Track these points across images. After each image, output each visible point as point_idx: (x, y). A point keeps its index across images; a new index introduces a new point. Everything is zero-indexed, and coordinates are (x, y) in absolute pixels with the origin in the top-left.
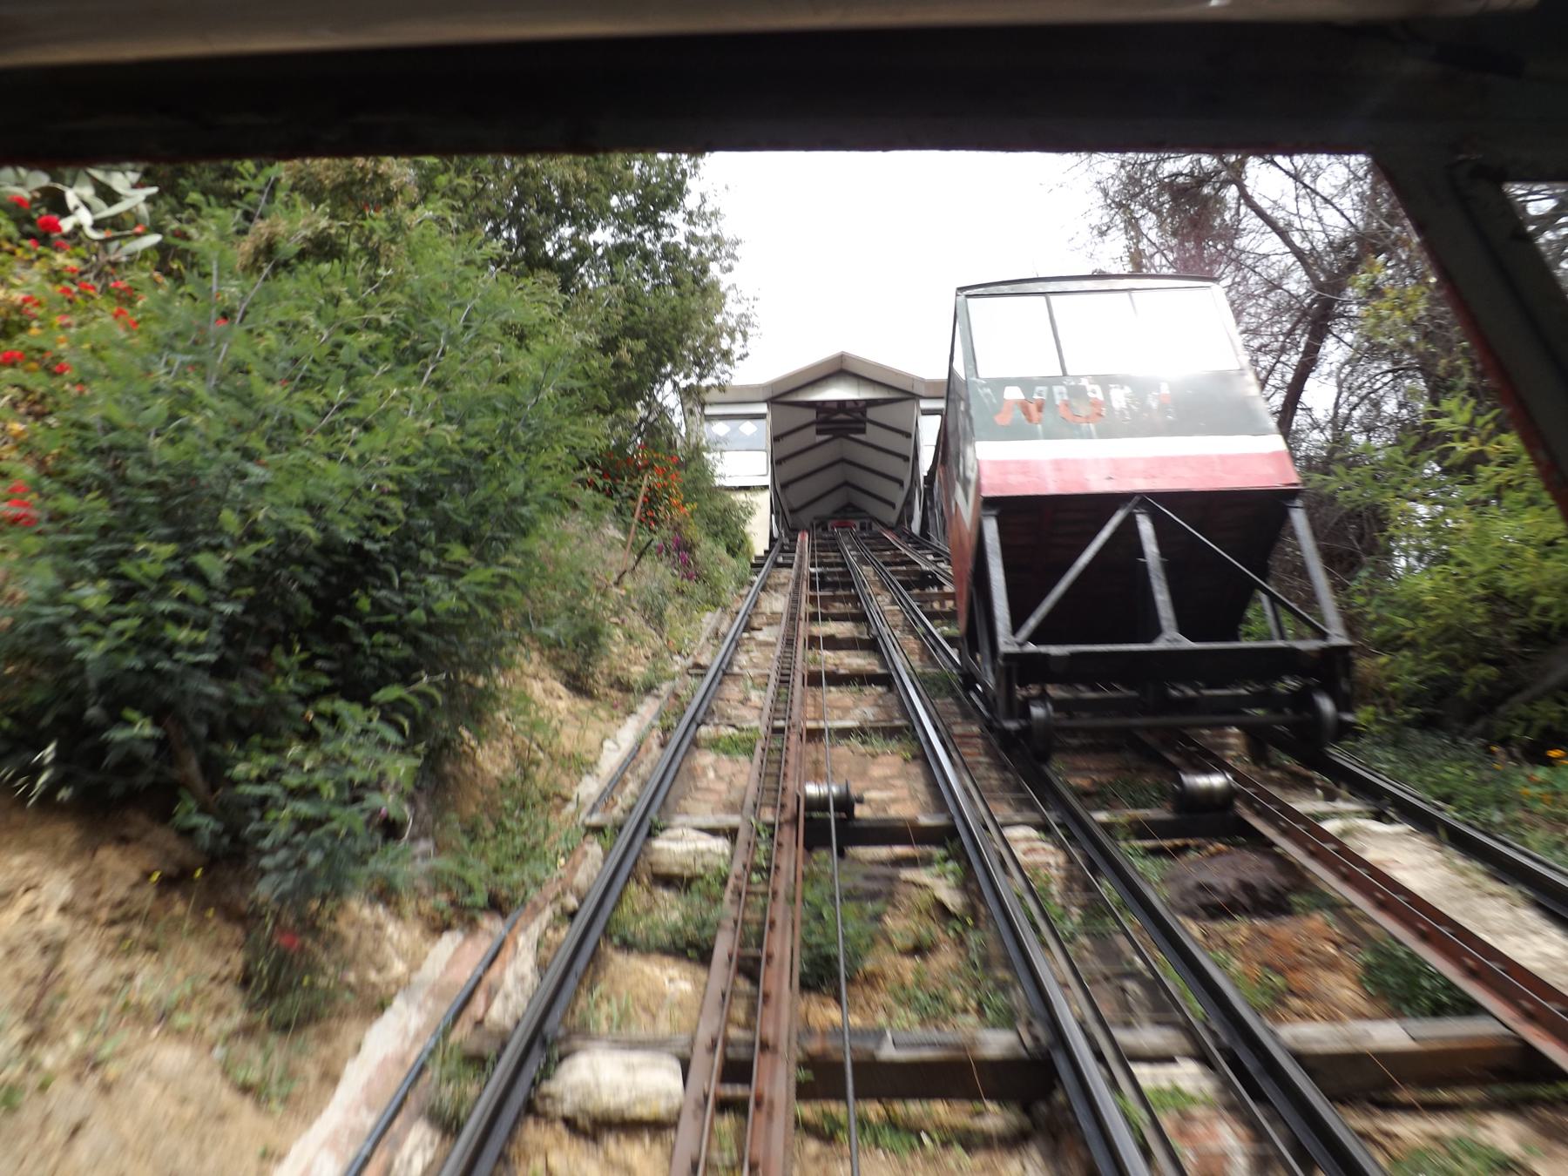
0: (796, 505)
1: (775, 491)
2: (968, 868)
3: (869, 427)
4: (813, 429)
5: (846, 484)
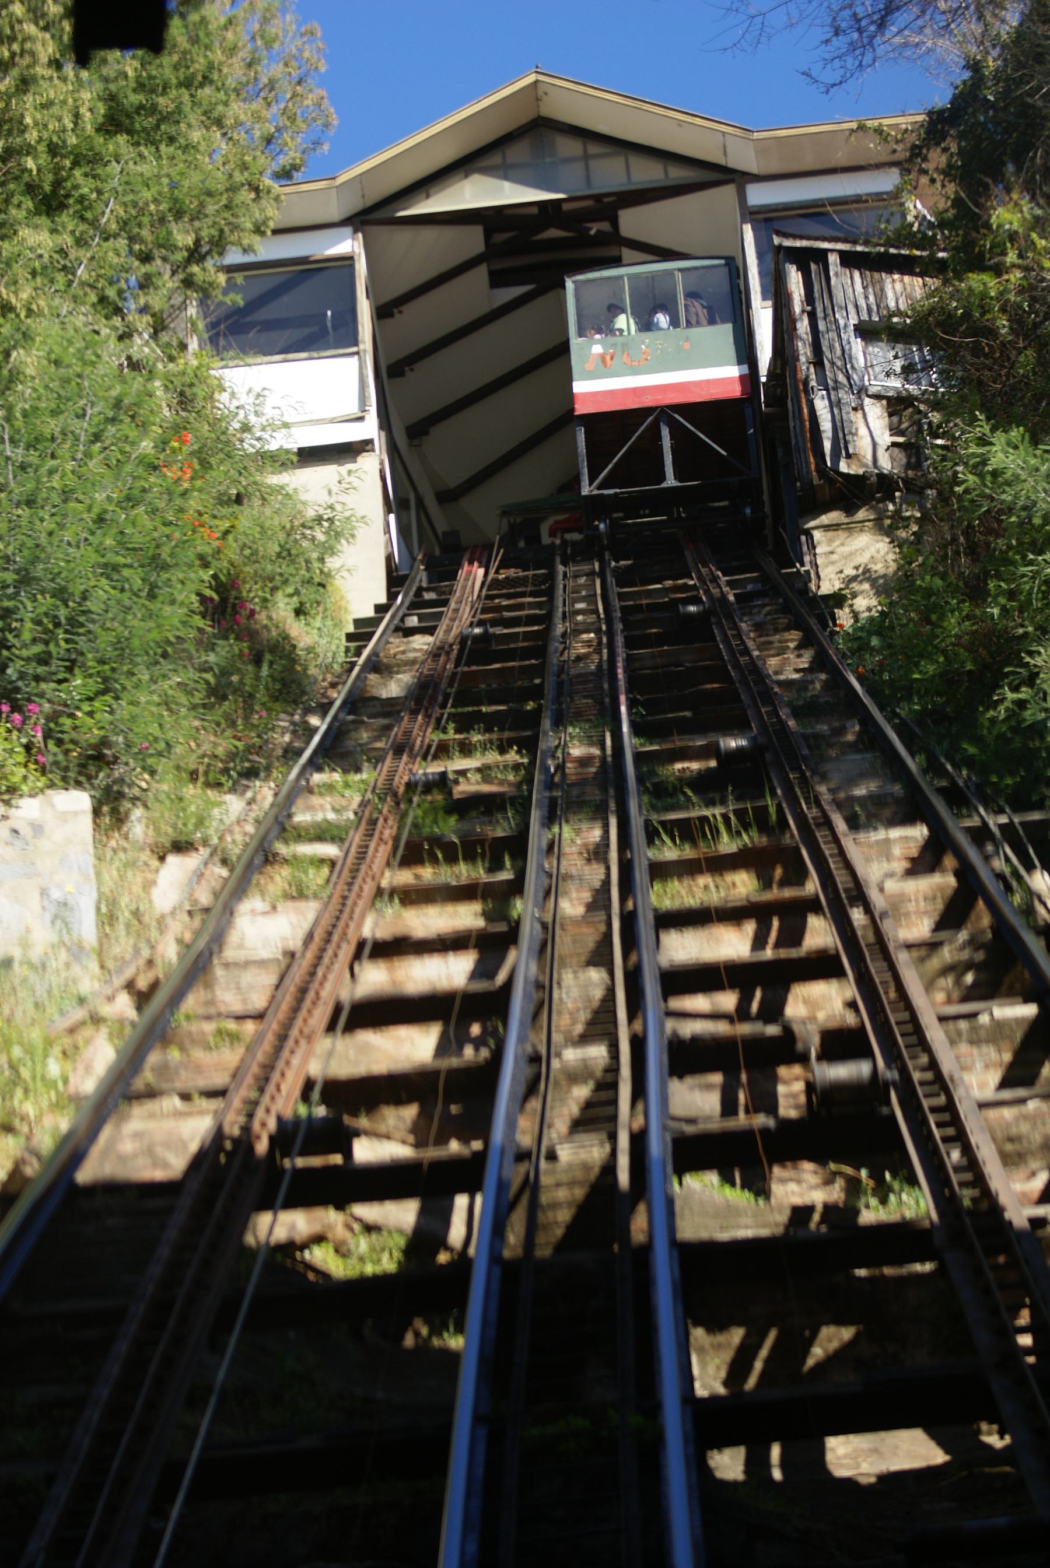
0: (453, 480)
1: (393, 449)
4: (481, 273)
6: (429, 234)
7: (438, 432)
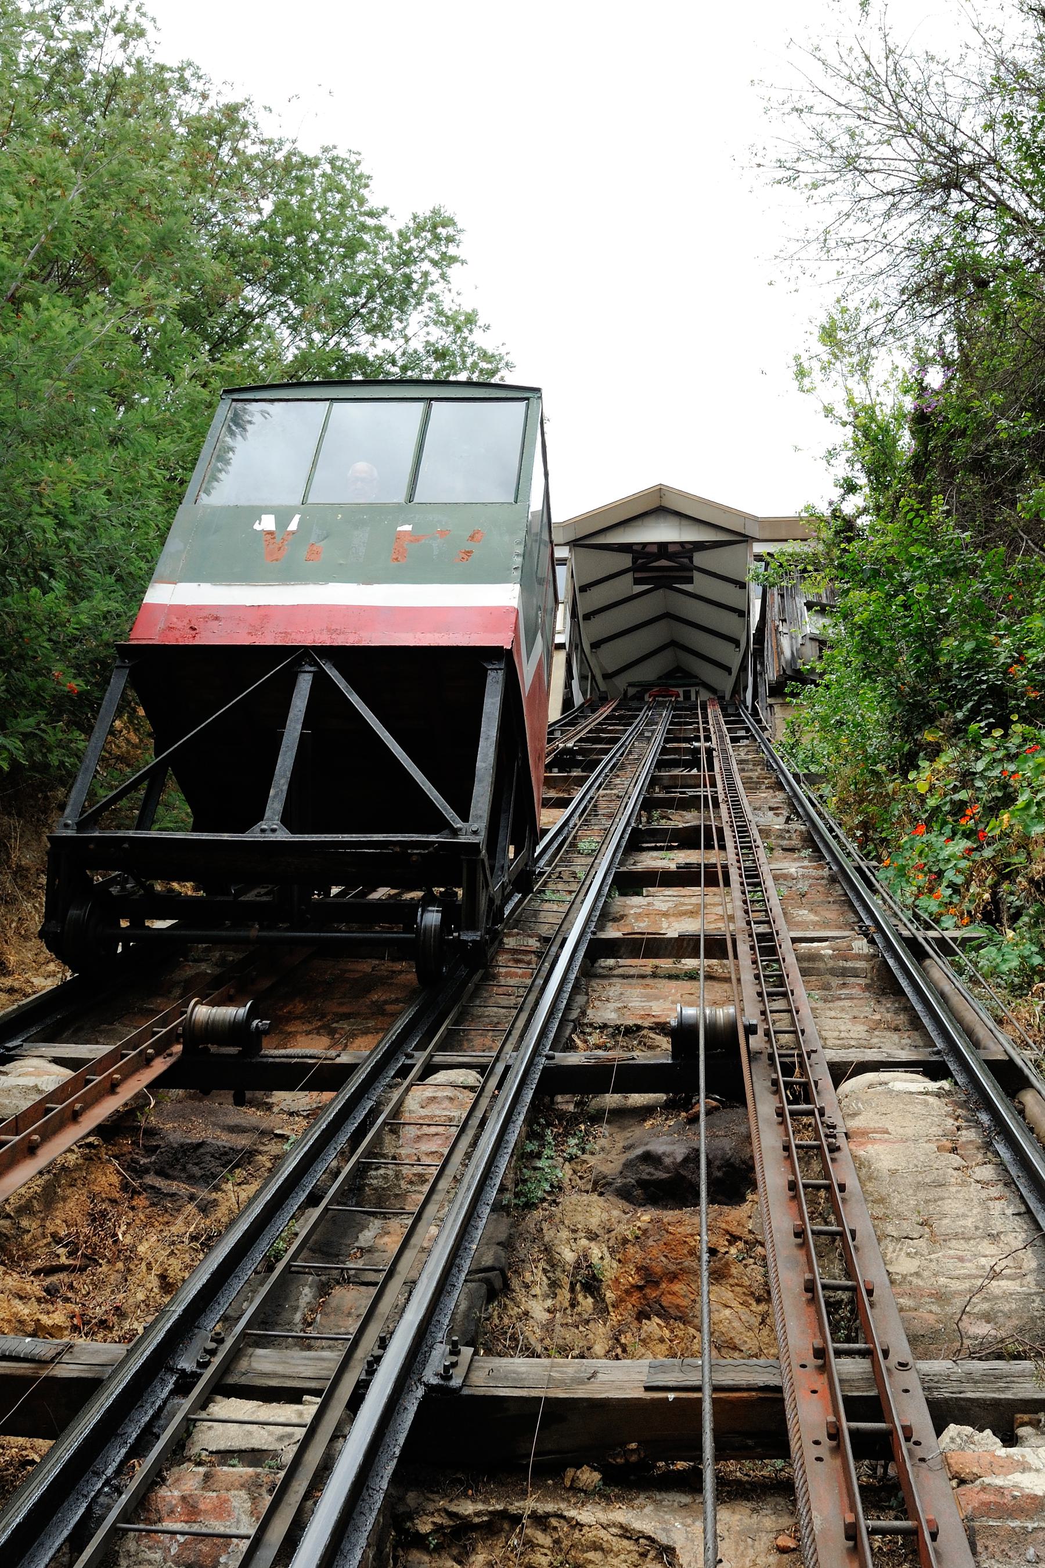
0: (735, 616)
2: (817, 849)
3: (696, 575)
4: (629, 577)
5: (673, 644)
6: (607, 555)
7: (604, 647)
